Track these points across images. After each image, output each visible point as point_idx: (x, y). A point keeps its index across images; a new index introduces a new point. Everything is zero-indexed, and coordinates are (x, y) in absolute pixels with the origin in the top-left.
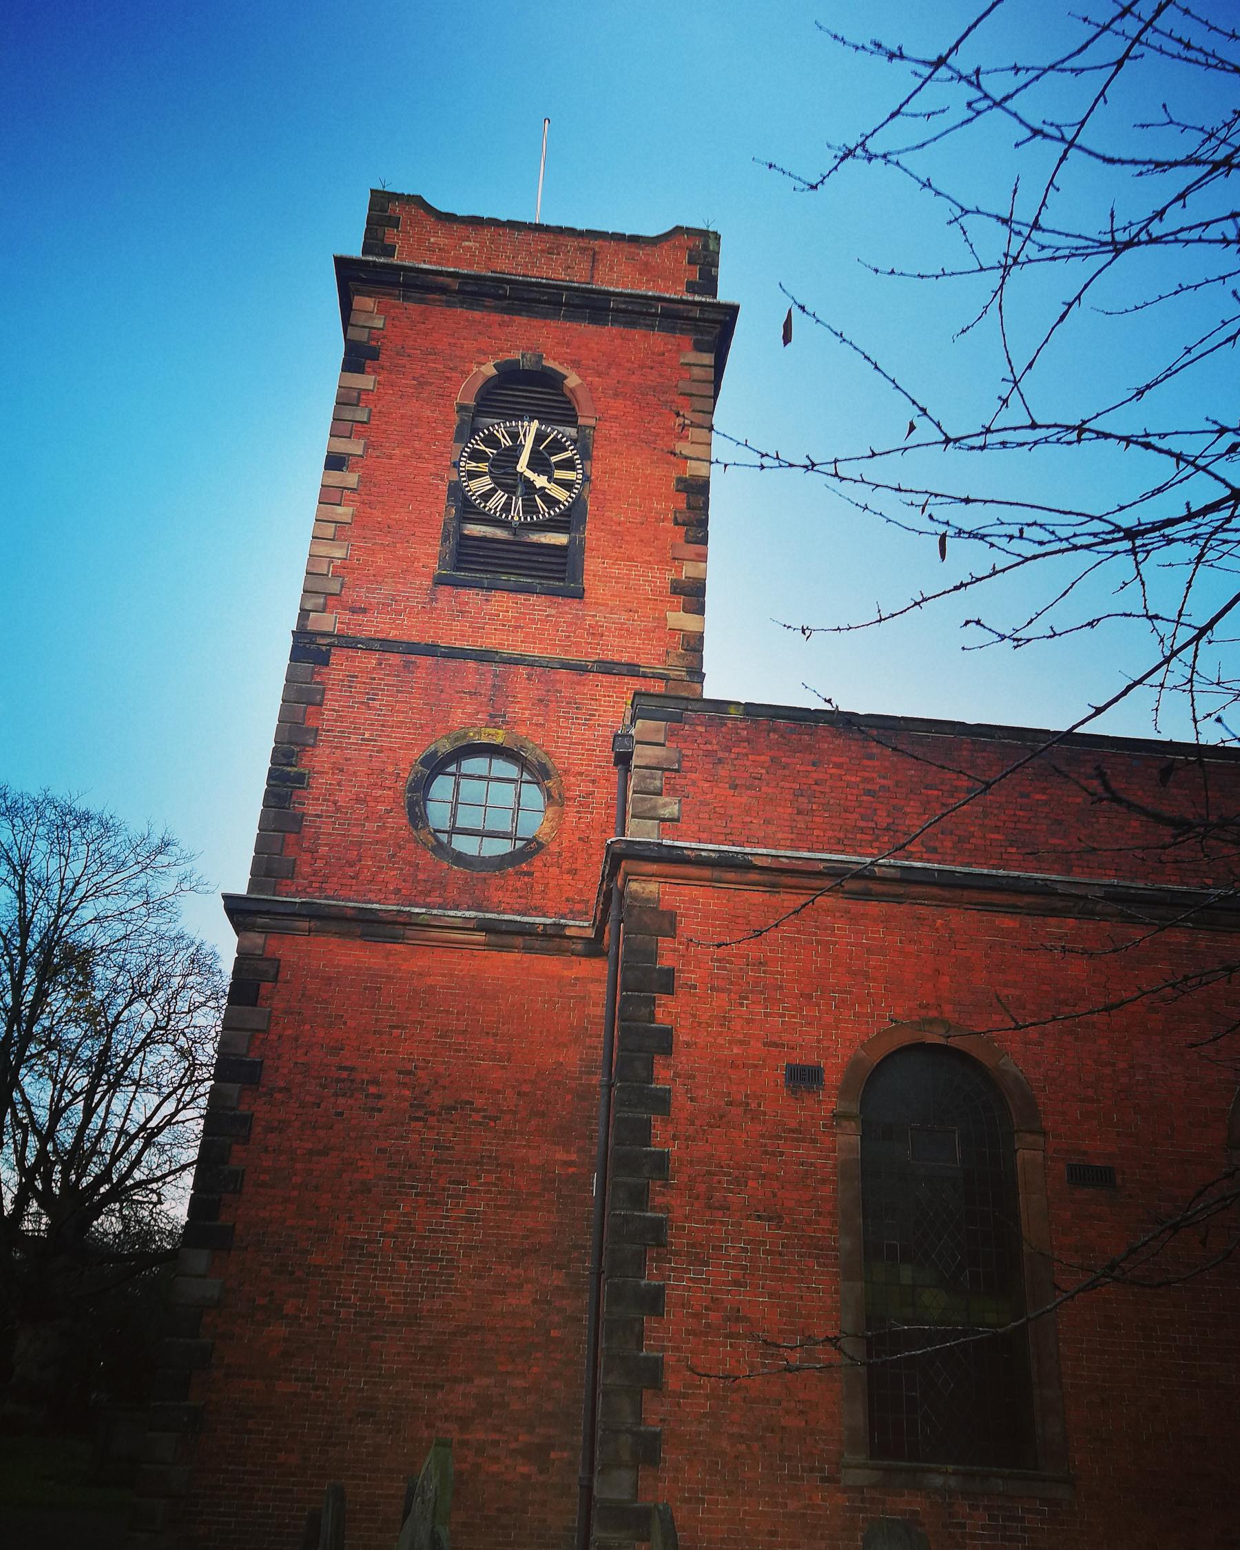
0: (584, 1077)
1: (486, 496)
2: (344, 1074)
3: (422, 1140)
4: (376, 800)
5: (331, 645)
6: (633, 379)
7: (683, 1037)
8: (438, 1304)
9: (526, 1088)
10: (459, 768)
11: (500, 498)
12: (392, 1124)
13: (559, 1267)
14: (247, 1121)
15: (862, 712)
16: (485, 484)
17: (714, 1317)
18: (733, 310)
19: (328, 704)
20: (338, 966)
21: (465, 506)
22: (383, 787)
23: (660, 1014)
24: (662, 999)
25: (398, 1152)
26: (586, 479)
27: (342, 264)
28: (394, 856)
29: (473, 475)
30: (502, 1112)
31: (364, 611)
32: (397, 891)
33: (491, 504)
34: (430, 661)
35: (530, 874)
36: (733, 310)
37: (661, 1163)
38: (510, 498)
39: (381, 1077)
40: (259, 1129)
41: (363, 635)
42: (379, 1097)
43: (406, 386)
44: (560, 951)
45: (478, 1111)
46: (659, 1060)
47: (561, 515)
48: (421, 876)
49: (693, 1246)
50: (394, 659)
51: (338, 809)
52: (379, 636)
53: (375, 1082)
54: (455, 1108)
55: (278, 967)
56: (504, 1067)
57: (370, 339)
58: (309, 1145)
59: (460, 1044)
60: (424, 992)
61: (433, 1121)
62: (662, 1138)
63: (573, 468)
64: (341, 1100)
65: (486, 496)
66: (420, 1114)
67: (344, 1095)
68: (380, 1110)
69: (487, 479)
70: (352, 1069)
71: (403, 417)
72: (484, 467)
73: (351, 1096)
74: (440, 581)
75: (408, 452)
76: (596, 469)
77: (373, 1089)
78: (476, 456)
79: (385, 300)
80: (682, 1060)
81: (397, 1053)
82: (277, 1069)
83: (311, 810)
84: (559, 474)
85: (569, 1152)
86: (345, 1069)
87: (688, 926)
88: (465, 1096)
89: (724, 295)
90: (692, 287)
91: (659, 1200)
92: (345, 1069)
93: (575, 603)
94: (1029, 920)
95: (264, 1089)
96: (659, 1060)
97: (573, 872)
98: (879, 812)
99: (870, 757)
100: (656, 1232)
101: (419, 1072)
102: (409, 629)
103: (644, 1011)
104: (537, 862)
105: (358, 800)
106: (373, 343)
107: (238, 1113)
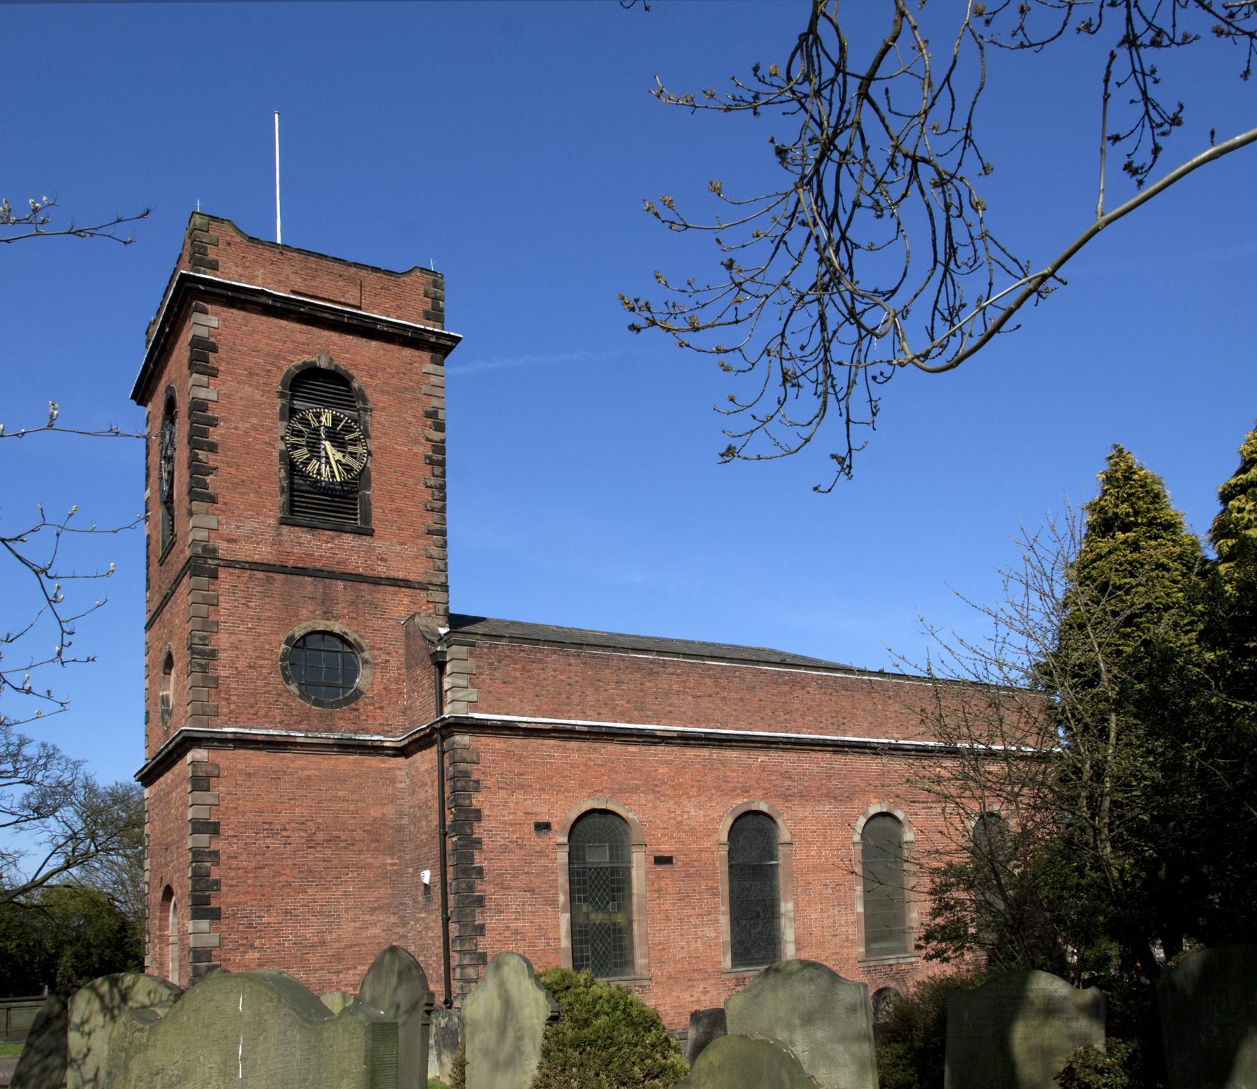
2: (266, 826)
4: (261, 666)
5: (218, 565)
6: (394, 381)
7: (486, 812)
8: (335, 936)
9: (368, 828)
13: (394, 914)
17: (507, 934)
19: (222, 605)
22: (264, 659)
23: (474, 802)
24: (475, 795)
31: (235, 541)
32: (281, 722)
33: (310, 468)
34: (283, 576)
35: (357, 710)
37: (480, 871)
41: (238, 558)
43: (241, 375)
46: (476, 824)
48: (294, 713)
50: (260, 575)
51: (239, 673)
52: (249, 559)
53: (285, 829)
57: (210, 335)
62: (479, 860)
64: (268, 840)
71: (241, 398)
72: (302, 441)
74: (283, 522)
75: (248, 425)
76: (372, 445)
77: (284, 833)
80: (485, 824)
83: (222, 673)
84: (350, 448)
87: (486, 757)
88: (335, 833)
90: (428, 316)
91: (479, 888)
93: (368, 538)
94: (644, 748)
96: (476, 824)
97: (381, 708)
99: (570, 665)
100: (480, 901)
102: (264, 553)
103: (467, 802)
104: (361, 703)
105: (250, 667)
106: (212, 340)
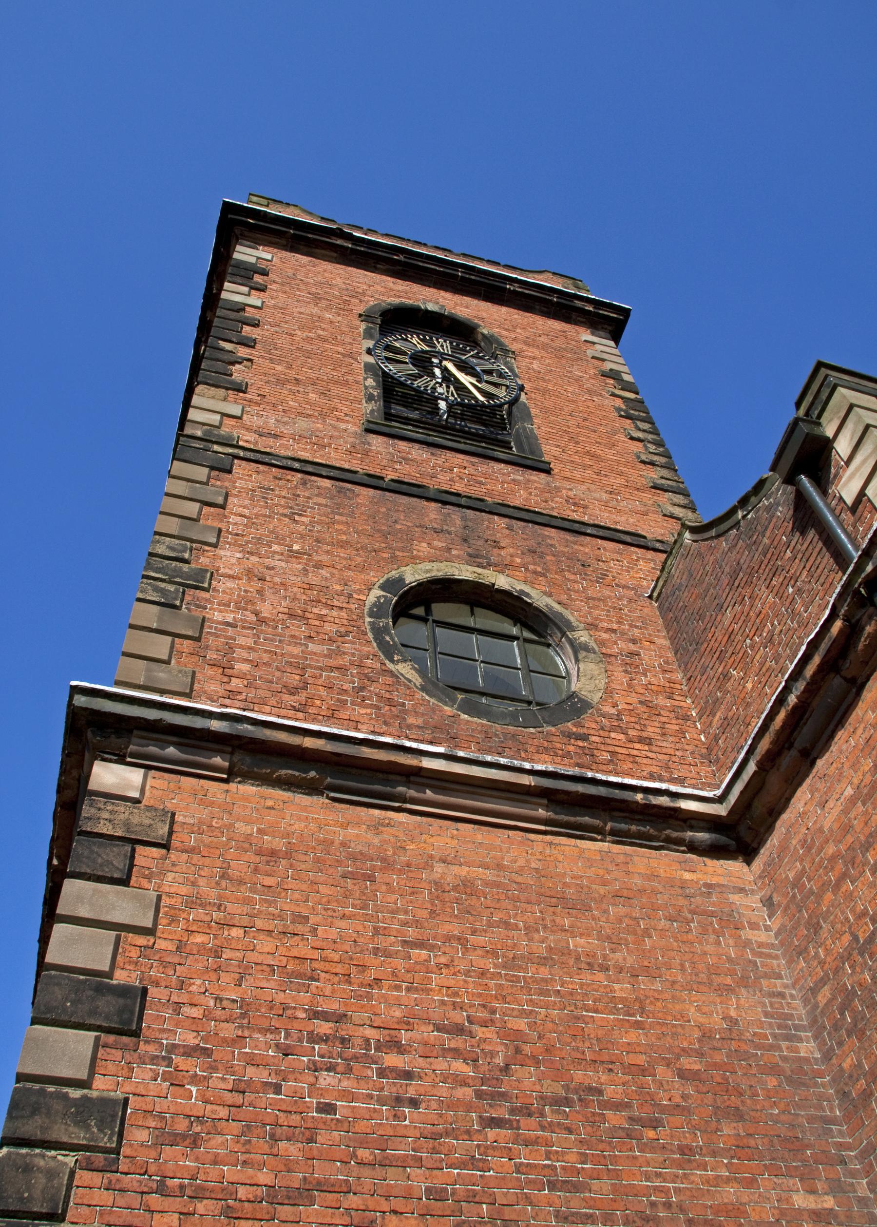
0: (784, 1044)
2: (324, 1028)
3: (518, 1169)
10: (428, 611)
12: (447, 1134)
14: (113, 1113)
20: (288, 835)
25: (473, 1198)
28: (362, 688)
30: (663, 1109)
39: (404, 1037)
40: (142, 1135)
42: (408, 1075)
44: (671, 843)
45: (618, 1106)
49: (303, 974)
54: (568, 1102)
55: (172, 822)
56: (638, 1025)
58: (265, 1177)
59: (545, 981)
60: (455, 888)
61: (529, 1127)
64: (326, 1079)
66: (501, 1112)
67: (331, 1068)
68: (414, 1103)
70: (340, 1018)
73: (349, 1070)
81: (428, 991)
82: (178, 1006)
85: (813, 1191)
86: (324, 1016)
92: (324, 1016)
95: (152, 1049)
98: (171, 947)
101: (480, 1032)
107: (94, 1094)
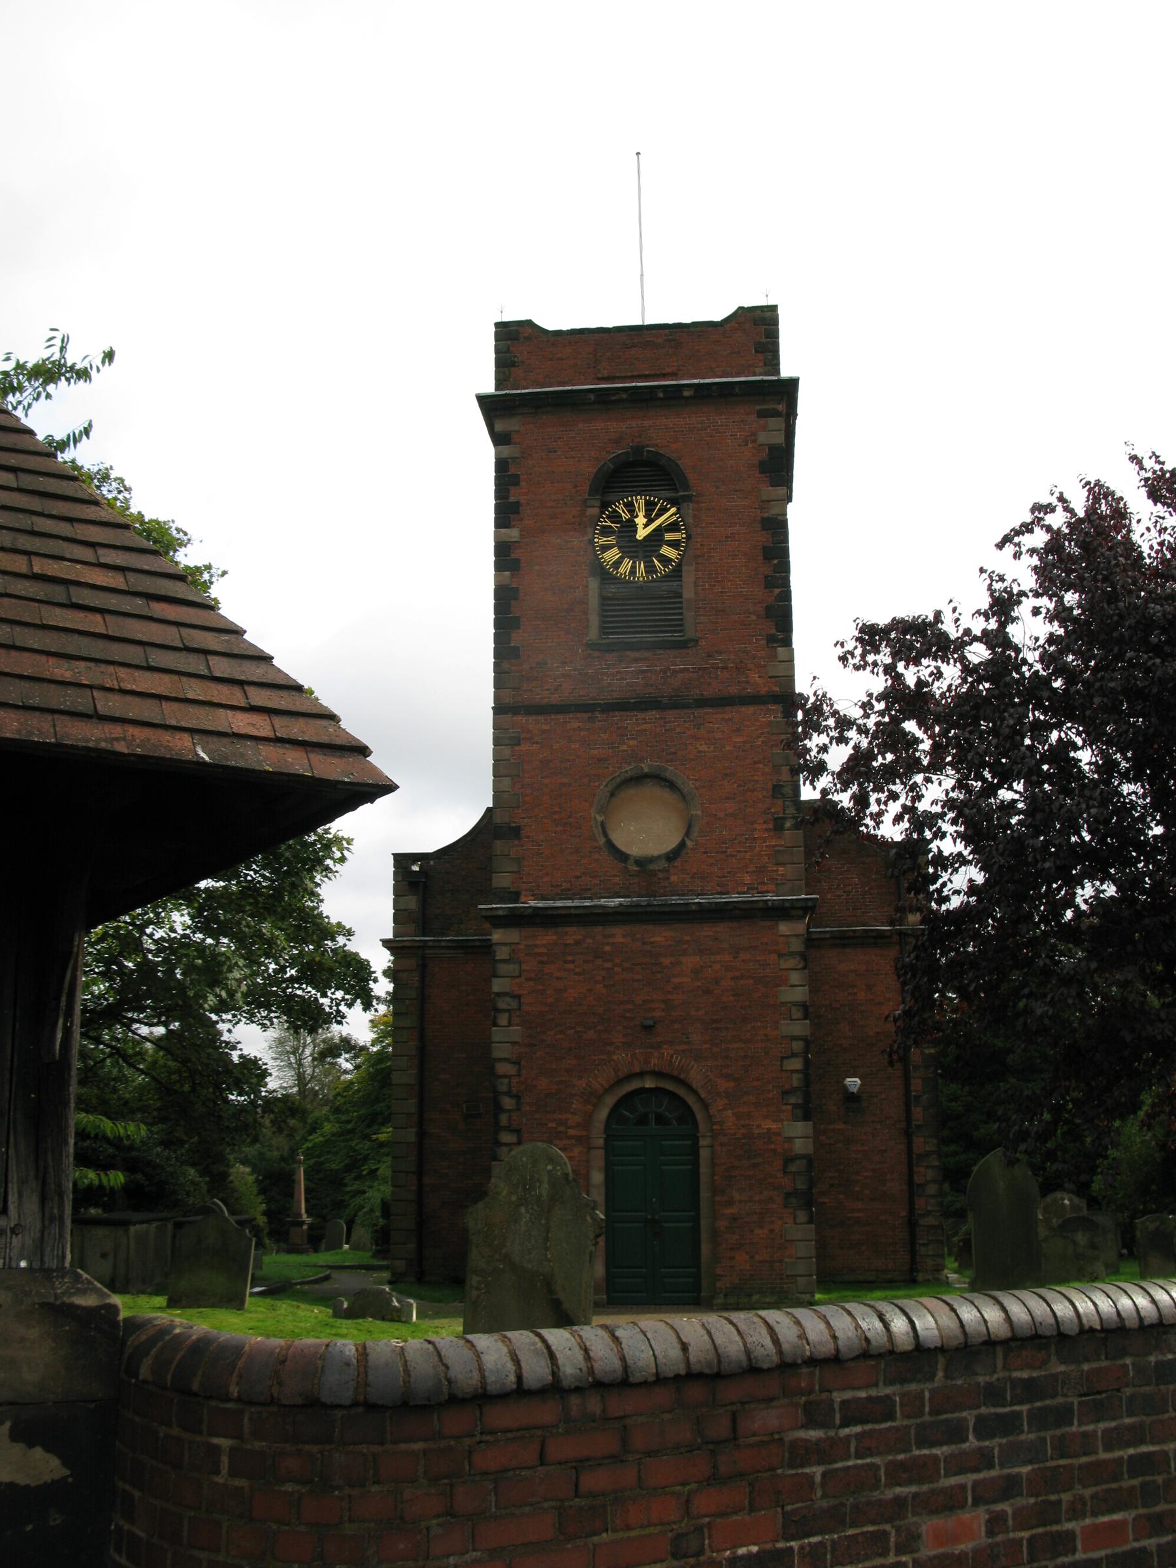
1: (617, 564)
2: (569, 958)
11: (627, 565)
15: (565, 328)
16: (613, 555)
18: (793, 384)
21: (603, 579)
26: (689, 537)
27: (483, 400)
29: (605, 548)
33: (621, 570)
36: (793, 384)
38: (634, 563)
47: (673, 571)
63: (678, 530)
65: (617, 564)
69: (615, 550)
72: (612, 539)
78: (606, 532)
79: (560, 929)
89: (786, 372)
